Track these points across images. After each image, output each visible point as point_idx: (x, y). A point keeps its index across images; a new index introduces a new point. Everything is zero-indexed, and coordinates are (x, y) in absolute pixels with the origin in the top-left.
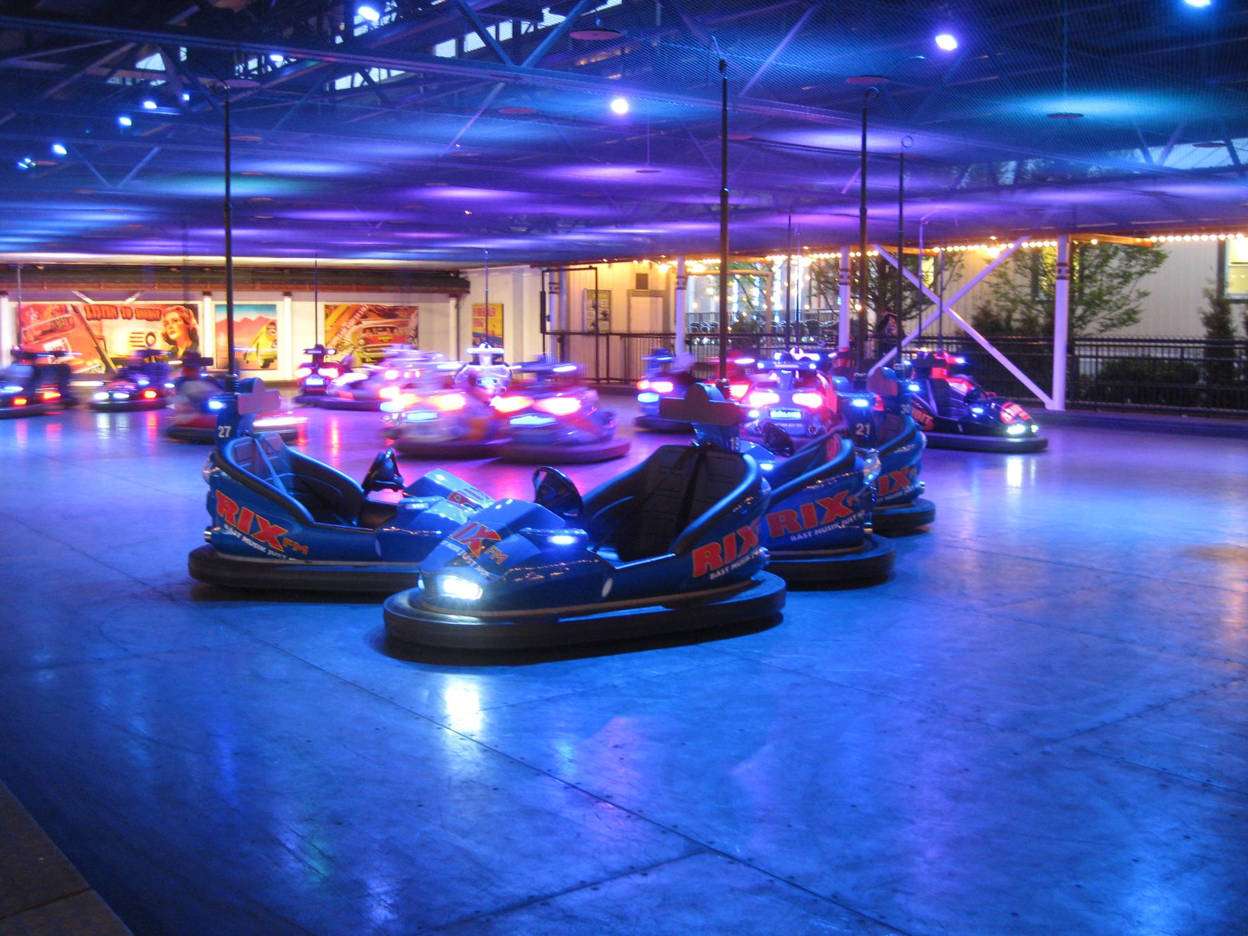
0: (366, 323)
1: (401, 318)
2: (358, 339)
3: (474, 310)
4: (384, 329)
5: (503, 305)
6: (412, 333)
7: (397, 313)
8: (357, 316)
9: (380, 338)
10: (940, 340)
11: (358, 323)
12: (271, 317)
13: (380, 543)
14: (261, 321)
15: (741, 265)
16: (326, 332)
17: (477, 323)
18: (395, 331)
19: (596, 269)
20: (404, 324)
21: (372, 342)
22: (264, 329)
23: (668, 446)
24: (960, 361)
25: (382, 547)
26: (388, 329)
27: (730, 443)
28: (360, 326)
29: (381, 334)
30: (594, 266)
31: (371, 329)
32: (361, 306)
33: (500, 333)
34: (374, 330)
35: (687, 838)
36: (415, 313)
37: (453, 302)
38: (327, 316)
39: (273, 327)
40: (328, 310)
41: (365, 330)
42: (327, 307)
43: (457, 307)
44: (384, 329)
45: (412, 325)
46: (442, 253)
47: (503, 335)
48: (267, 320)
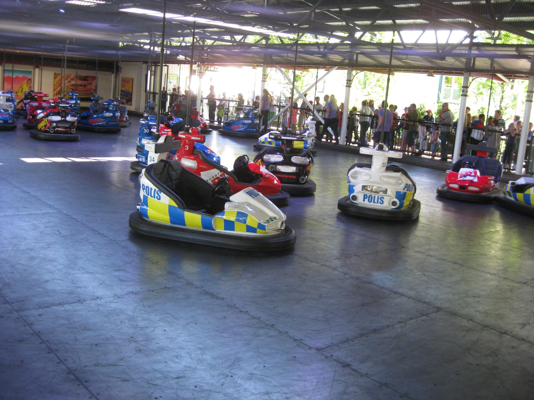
1: (89, 81)
2: (69, 89)
4: (81, 85)
5: (133, 79)
7: (87, 79)
8: (69, 79)
9: (79, 89)
10: (22, 101)
11: (69, 82)
12: (29, 76)
14: (24, 78)
16: (54, 85)
18: (86, 87)
19: (168, 66)
20: (90, 84)
22: (26, 82)
23: (470, 194)
24: (307, 177)
26: (83, 86)
28: (70, 83)
29: (79, 87)
31: (75, 85)
32: (71, 75)
33: (131, 91)
34: (77, 86)
39: (30, 81)
40: (56, 76)
41: (72, 85)
43: (116, 77)
45: (94, 84)
46: (55, 53)
47: (132, 92)
48: (27, 78)
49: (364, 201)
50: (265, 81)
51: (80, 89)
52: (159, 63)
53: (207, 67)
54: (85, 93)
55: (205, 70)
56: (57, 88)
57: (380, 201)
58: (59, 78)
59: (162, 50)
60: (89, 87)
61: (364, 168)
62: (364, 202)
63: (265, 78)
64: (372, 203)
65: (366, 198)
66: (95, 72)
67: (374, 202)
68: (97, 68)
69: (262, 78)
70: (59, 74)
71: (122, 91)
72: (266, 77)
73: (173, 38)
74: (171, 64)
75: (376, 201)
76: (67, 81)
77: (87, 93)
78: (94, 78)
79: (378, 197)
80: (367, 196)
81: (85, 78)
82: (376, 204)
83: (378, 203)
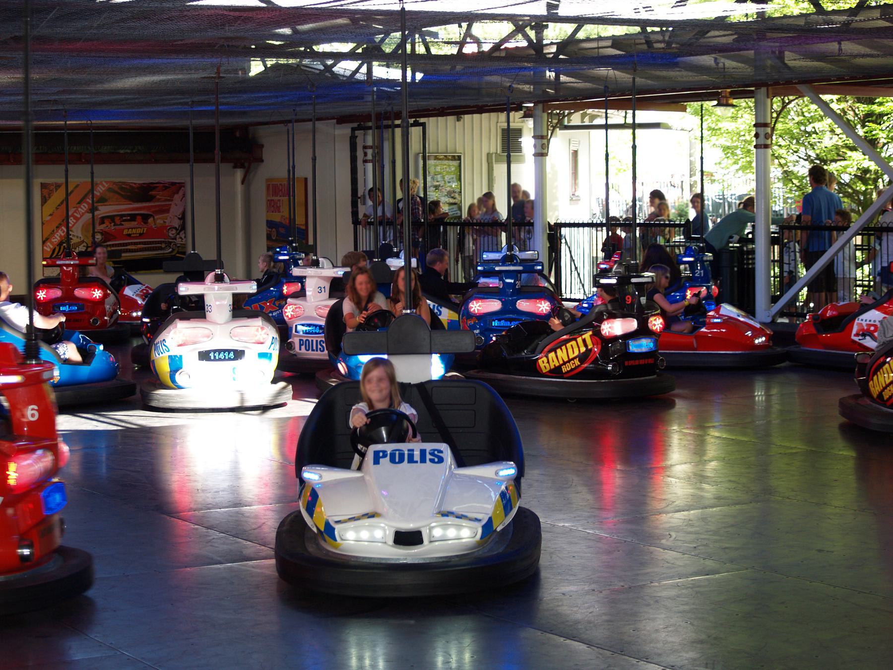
0: (104, 210)
1: (158, 200)
3: (268, 187)
4: (133, 218)
6: (176, 223)
9: (125, 232)
13: (696, 340)
15: (178, 241)
17: (272, 206)
18: (151, 220)
19: (423, 125)
21: (115, 239)
25: (697, 343)
27: (874, 281)
29: (127, 225)
30: (422, 120)
31: (112, 218)
34: (117, 219)
35: (767, 39)
36: (181, 193)
37: (239, 174)
38: (44, 200)
40: (46, 191)
42: (43, 186)
44: (133, 218)
45: (176, 210)
49: (300, 349)
50: (766, 146)
51: (130, 231)
52: (370, 120)
53: (558, 114)
54: (145, 243)
55: (554, 128)
56: (53, 233)
57: (319, 347)
58: (58, 197)
59: (217, 108)
60: (159, 221)
61: (300, 298)
62: (300, 351)
63: (769, 136)
64: (310, 351)
65: (303, 345)
66: (186, 166)
67: (313, 350)
68: (217, 152)
69: (535, 146)
70: (58, 186)
71: (270, 224)
72: (769, 130)
73: (433, 29)
74: (431, 119)
75: (315, 348)
76: (84, 207)
77: (151, 243)
78: (176, 187)
79: (317, 341)
80: (303, 340)
81: (143, 193)
82: (315, 352)
83: (317, 351)
